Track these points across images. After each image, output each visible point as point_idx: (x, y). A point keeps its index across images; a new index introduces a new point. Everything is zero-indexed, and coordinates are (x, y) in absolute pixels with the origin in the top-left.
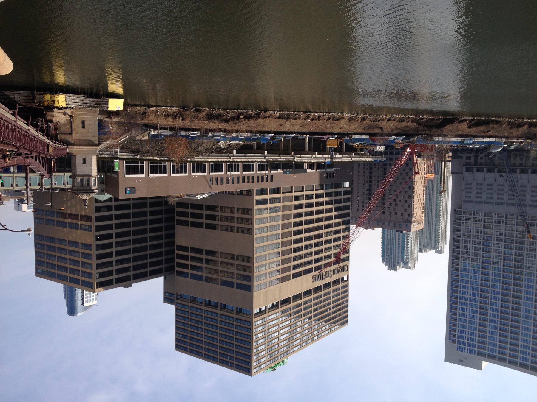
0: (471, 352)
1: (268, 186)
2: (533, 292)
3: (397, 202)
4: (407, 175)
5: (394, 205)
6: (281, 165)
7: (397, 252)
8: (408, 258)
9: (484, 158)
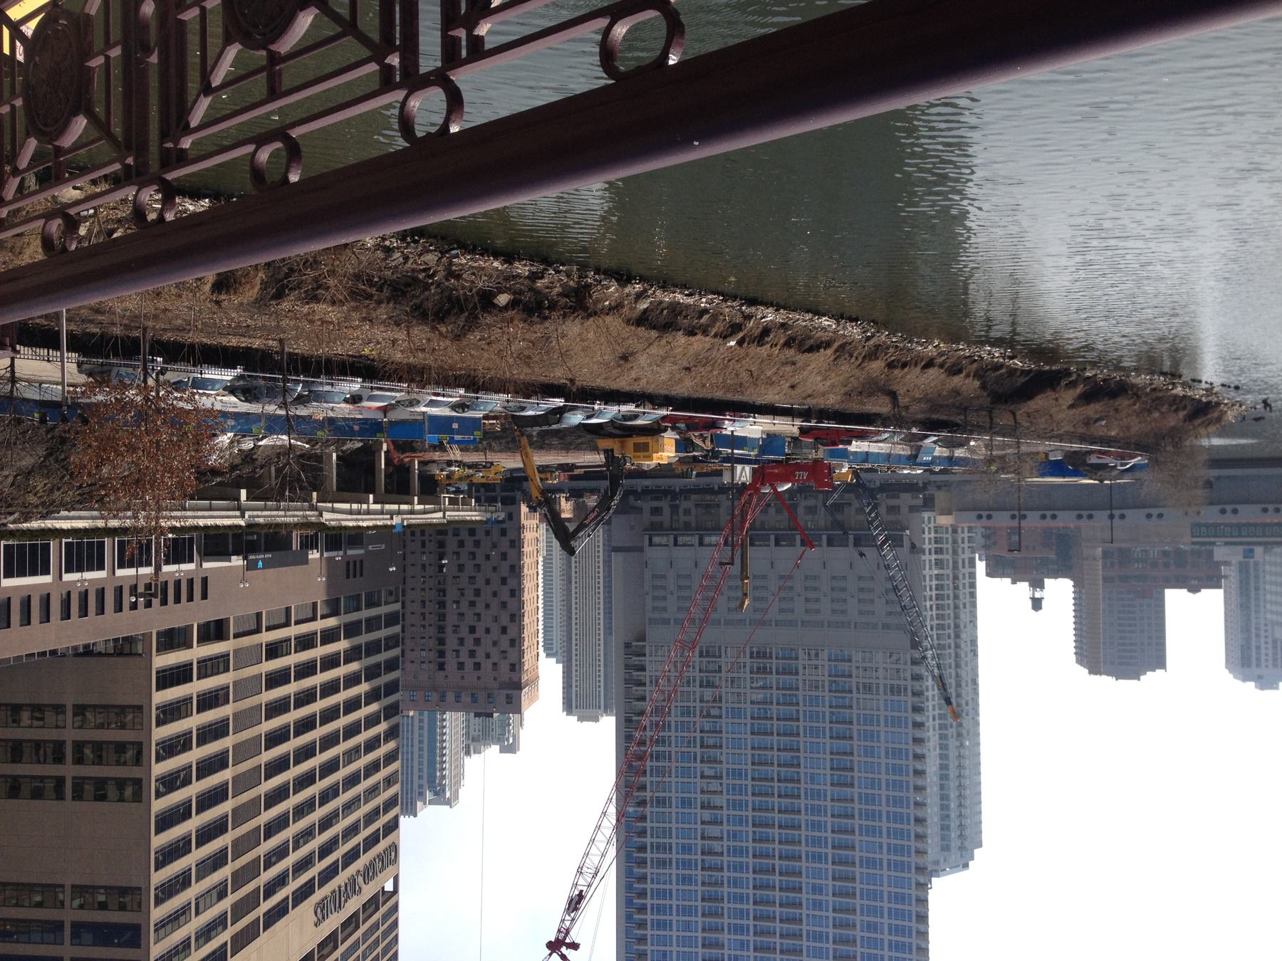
1: (192, 615)
2: (826, 838)
3: (480, 633)
4: (505, 559)
5: (472, 642)
6: (230, 541)
7: (416, 764)
8: (443, 777)
9: (693, 511)
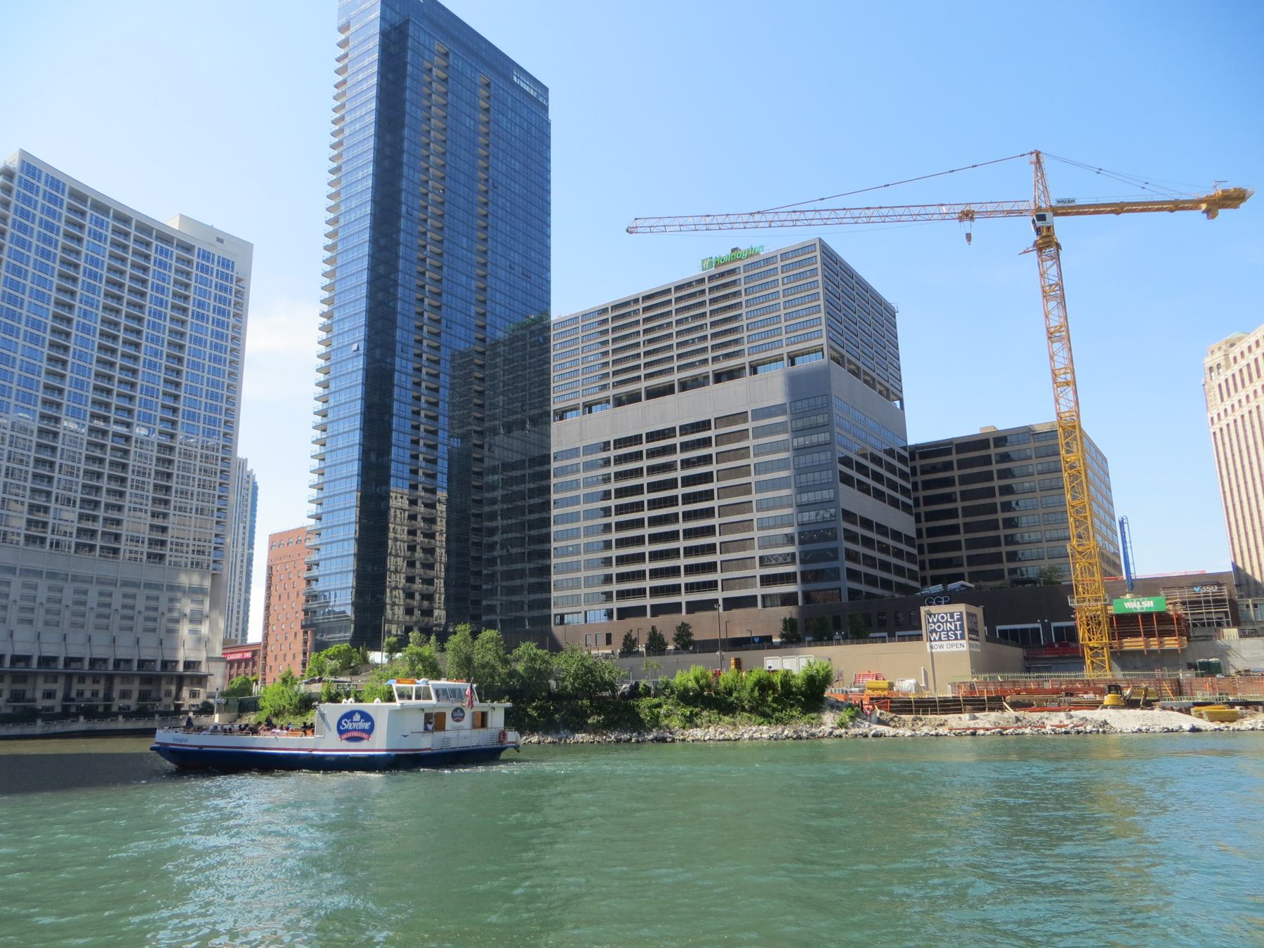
0: (206, 255)
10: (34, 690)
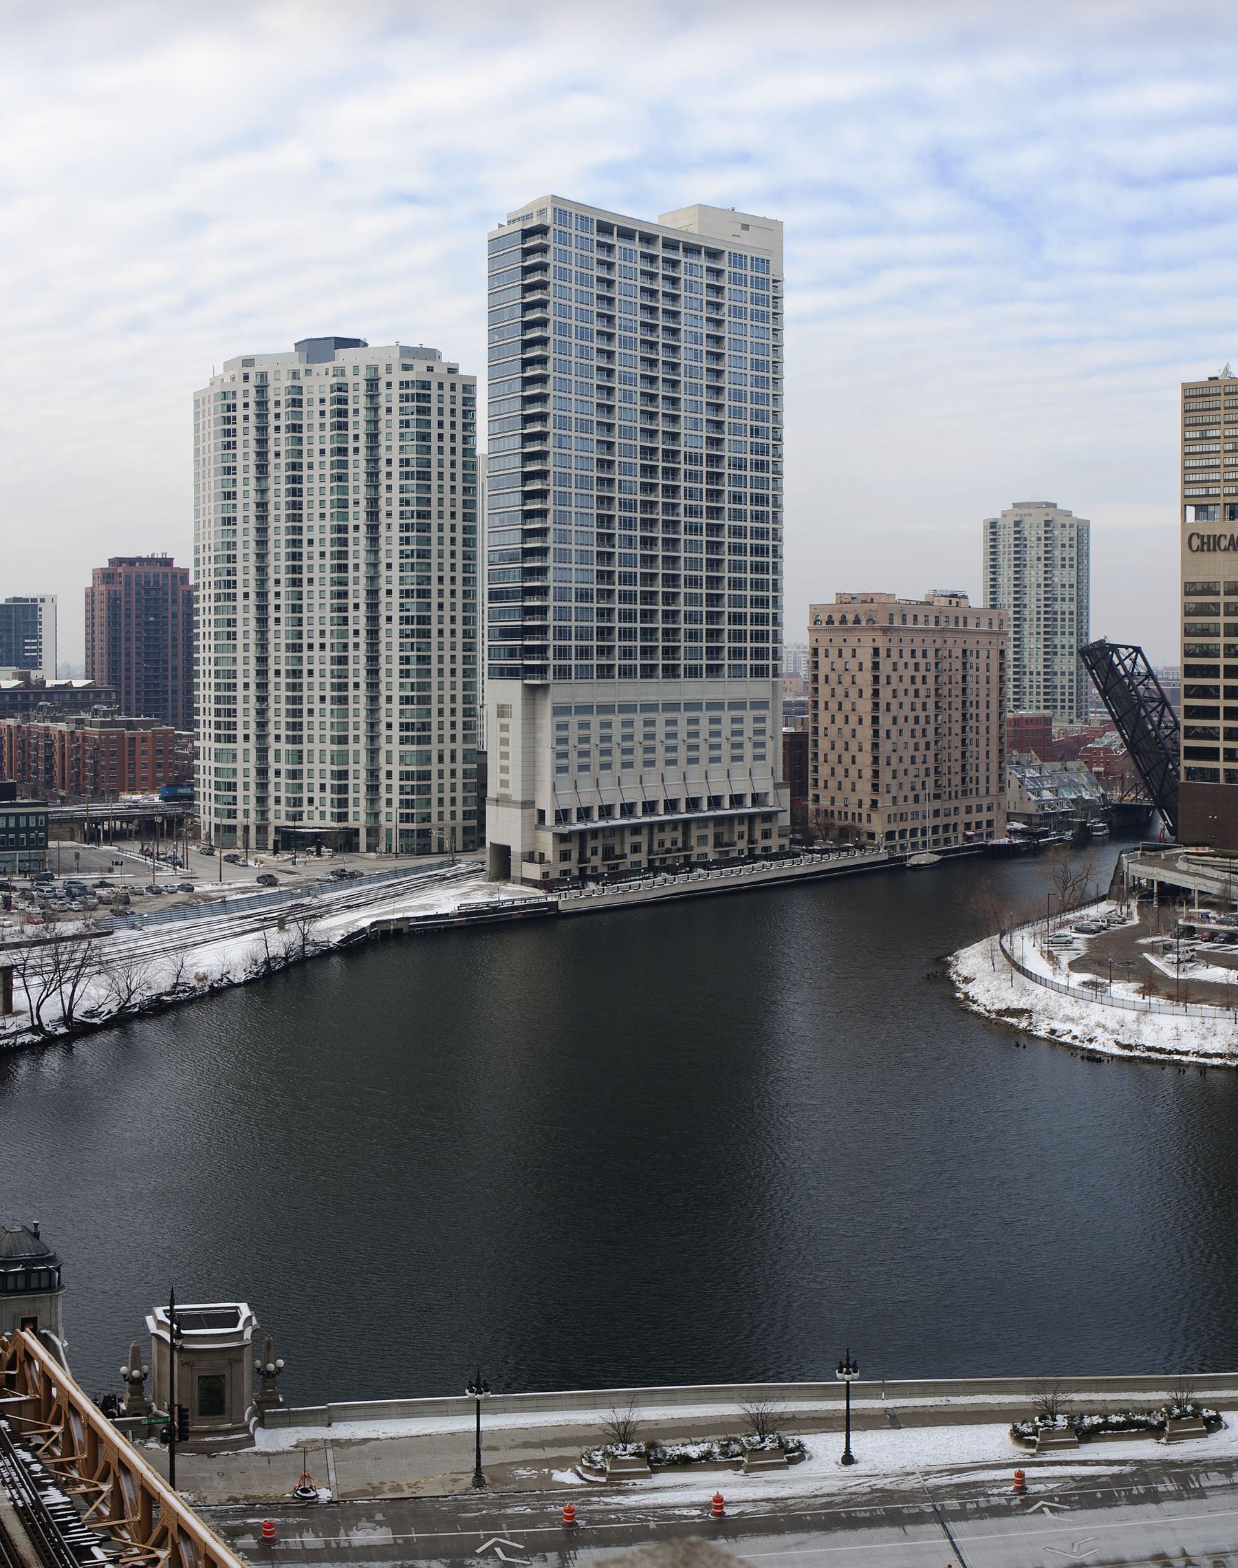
10: (623, 843)
